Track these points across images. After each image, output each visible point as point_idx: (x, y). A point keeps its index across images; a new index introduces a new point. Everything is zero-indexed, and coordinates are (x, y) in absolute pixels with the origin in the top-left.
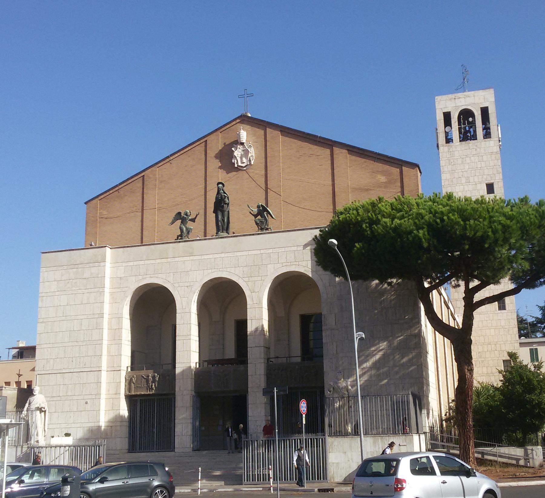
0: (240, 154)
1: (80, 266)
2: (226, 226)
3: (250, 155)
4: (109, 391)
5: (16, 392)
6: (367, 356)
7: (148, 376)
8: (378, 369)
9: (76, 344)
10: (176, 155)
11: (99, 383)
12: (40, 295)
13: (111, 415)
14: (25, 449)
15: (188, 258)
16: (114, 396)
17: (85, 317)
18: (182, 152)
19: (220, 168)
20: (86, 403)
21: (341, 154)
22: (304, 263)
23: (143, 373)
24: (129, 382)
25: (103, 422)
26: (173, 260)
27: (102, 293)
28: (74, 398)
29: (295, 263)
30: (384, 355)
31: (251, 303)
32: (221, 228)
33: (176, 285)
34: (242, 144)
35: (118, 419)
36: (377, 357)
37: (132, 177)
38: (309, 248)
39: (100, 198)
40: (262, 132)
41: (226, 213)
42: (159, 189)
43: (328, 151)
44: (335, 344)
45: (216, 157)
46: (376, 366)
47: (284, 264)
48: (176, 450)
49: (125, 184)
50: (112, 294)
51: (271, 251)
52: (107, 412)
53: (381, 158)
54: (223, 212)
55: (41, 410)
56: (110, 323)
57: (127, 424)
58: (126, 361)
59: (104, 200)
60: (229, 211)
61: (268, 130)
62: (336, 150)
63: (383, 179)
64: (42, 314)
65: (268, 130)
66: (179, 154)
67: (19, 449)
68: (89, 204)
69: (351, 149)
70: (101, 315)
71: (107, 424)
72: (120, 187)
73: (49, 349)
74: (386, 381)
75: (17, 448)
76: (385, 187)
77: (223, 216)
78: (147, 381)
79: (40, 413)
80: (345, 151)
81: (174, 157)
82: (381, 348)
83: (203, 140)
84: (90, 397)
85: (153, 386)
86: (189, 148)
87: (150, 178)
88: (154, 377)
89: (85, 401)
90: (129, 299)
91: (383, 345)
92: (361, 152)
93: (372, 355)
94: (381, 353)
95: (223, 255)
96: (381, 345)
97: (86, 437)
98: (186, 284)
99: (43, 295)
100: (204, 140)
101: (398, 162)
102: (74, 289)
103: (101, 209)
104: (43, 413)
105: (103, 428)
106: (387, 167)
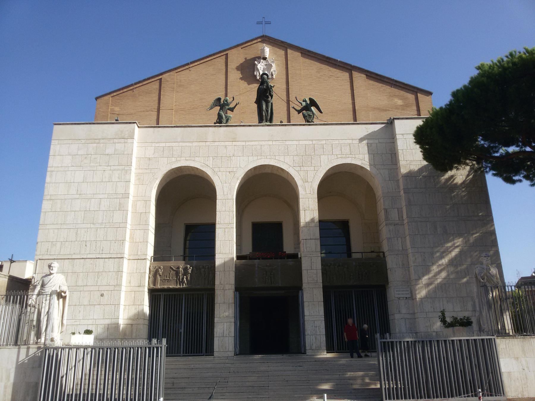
0: (262, 67)
1: (102, 141)
2: (269, 117)
3: (272, 70)
4: (130, 282)
5: (7, 280)
6: (443, 252)
7: (178, 268)
8: (456, 266)
9: (92, 226)
10: (196, 64)
11: (119, 272)
12: (49, 169)
13: (133, 311)
14: (32, 351)
15: (230, 143)
16: (137, 289)
17: (106, 196)
18: (202, 61)
19: (241, 79)
20: (102, 295)
21: (359, 79)
22: (361, 156)
23: (172, 264)
24: (155, 274)
25: (122, 321)
26: (213, 144)
27: (128, 172)
28: (86, 289)
29: (350, 156)
30: (461, 252)
31: (304, 193)
32: (264, 118)
33: (216, 170)
34: (265, 59)
35: (139, 315)
36: (453, 254)
37: (149, 79)
38: (365, 142)
39: (112, 95)
40: (283, 52)
41: (270, 104)
42: (177, 92)
43: (346, 75)
44: (400, 239)
45: (238, 68)
46: (451, 262)
47: (339, 156)
48: (216, 354)
49: (140, 84)
50: (138, 175)
51: (324, 142)
52: (127, 307)
53: (398, 84)
54: (267, 102)
55: (60, 295)
56: (135, 205)
57: (147, 322)
58: (150, 252)
59: (117, 97)
60: (272, 103)
61: (289, 51)
62: (355, 74)
63: (400, 102)
64: (50, 190)
65: (289, 51)
66: (198, 63)
67: (23, 350)
68: (99, 101)
69: (368, 74)
70: (126, 196)
71: (126, 322)
72: (135, 86)
73: (56, 231)
74: (465, 280)
75: (19, 348)
76: (403, 109)
77: (267, 106)
78: (177, 273)
79: (58, 299)
80: (364, 76)
81: (194, 65)
82: (456, 245)
83: (224, 53)
84: (107, 288)
85: (185, 279)
86: (210, 58)
87: (168, 81)
88: (185, 269)
89: (99, 294)
90: (157, 182)
91: (459, 241)
92: (379, 78)
93: (447, 251)
94: (457, 250)
95: (270, 143)
96: (455, 241)
97: (101, 337)
98: (228, 170)
99: (53, 169)
100: (225, 53)
101: (412, 89)
102: (92, 164)
103: (112, 105)
104: (61, 300)
105: (121, 327)
106: (402, 93)
